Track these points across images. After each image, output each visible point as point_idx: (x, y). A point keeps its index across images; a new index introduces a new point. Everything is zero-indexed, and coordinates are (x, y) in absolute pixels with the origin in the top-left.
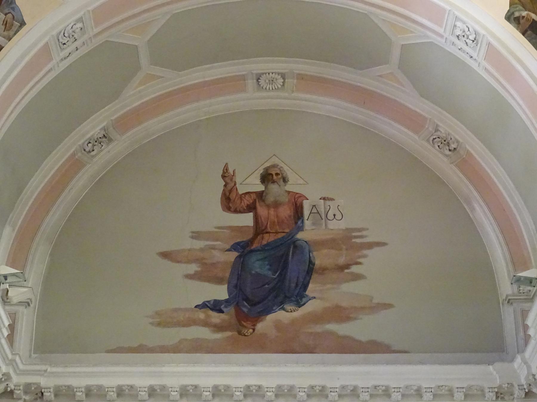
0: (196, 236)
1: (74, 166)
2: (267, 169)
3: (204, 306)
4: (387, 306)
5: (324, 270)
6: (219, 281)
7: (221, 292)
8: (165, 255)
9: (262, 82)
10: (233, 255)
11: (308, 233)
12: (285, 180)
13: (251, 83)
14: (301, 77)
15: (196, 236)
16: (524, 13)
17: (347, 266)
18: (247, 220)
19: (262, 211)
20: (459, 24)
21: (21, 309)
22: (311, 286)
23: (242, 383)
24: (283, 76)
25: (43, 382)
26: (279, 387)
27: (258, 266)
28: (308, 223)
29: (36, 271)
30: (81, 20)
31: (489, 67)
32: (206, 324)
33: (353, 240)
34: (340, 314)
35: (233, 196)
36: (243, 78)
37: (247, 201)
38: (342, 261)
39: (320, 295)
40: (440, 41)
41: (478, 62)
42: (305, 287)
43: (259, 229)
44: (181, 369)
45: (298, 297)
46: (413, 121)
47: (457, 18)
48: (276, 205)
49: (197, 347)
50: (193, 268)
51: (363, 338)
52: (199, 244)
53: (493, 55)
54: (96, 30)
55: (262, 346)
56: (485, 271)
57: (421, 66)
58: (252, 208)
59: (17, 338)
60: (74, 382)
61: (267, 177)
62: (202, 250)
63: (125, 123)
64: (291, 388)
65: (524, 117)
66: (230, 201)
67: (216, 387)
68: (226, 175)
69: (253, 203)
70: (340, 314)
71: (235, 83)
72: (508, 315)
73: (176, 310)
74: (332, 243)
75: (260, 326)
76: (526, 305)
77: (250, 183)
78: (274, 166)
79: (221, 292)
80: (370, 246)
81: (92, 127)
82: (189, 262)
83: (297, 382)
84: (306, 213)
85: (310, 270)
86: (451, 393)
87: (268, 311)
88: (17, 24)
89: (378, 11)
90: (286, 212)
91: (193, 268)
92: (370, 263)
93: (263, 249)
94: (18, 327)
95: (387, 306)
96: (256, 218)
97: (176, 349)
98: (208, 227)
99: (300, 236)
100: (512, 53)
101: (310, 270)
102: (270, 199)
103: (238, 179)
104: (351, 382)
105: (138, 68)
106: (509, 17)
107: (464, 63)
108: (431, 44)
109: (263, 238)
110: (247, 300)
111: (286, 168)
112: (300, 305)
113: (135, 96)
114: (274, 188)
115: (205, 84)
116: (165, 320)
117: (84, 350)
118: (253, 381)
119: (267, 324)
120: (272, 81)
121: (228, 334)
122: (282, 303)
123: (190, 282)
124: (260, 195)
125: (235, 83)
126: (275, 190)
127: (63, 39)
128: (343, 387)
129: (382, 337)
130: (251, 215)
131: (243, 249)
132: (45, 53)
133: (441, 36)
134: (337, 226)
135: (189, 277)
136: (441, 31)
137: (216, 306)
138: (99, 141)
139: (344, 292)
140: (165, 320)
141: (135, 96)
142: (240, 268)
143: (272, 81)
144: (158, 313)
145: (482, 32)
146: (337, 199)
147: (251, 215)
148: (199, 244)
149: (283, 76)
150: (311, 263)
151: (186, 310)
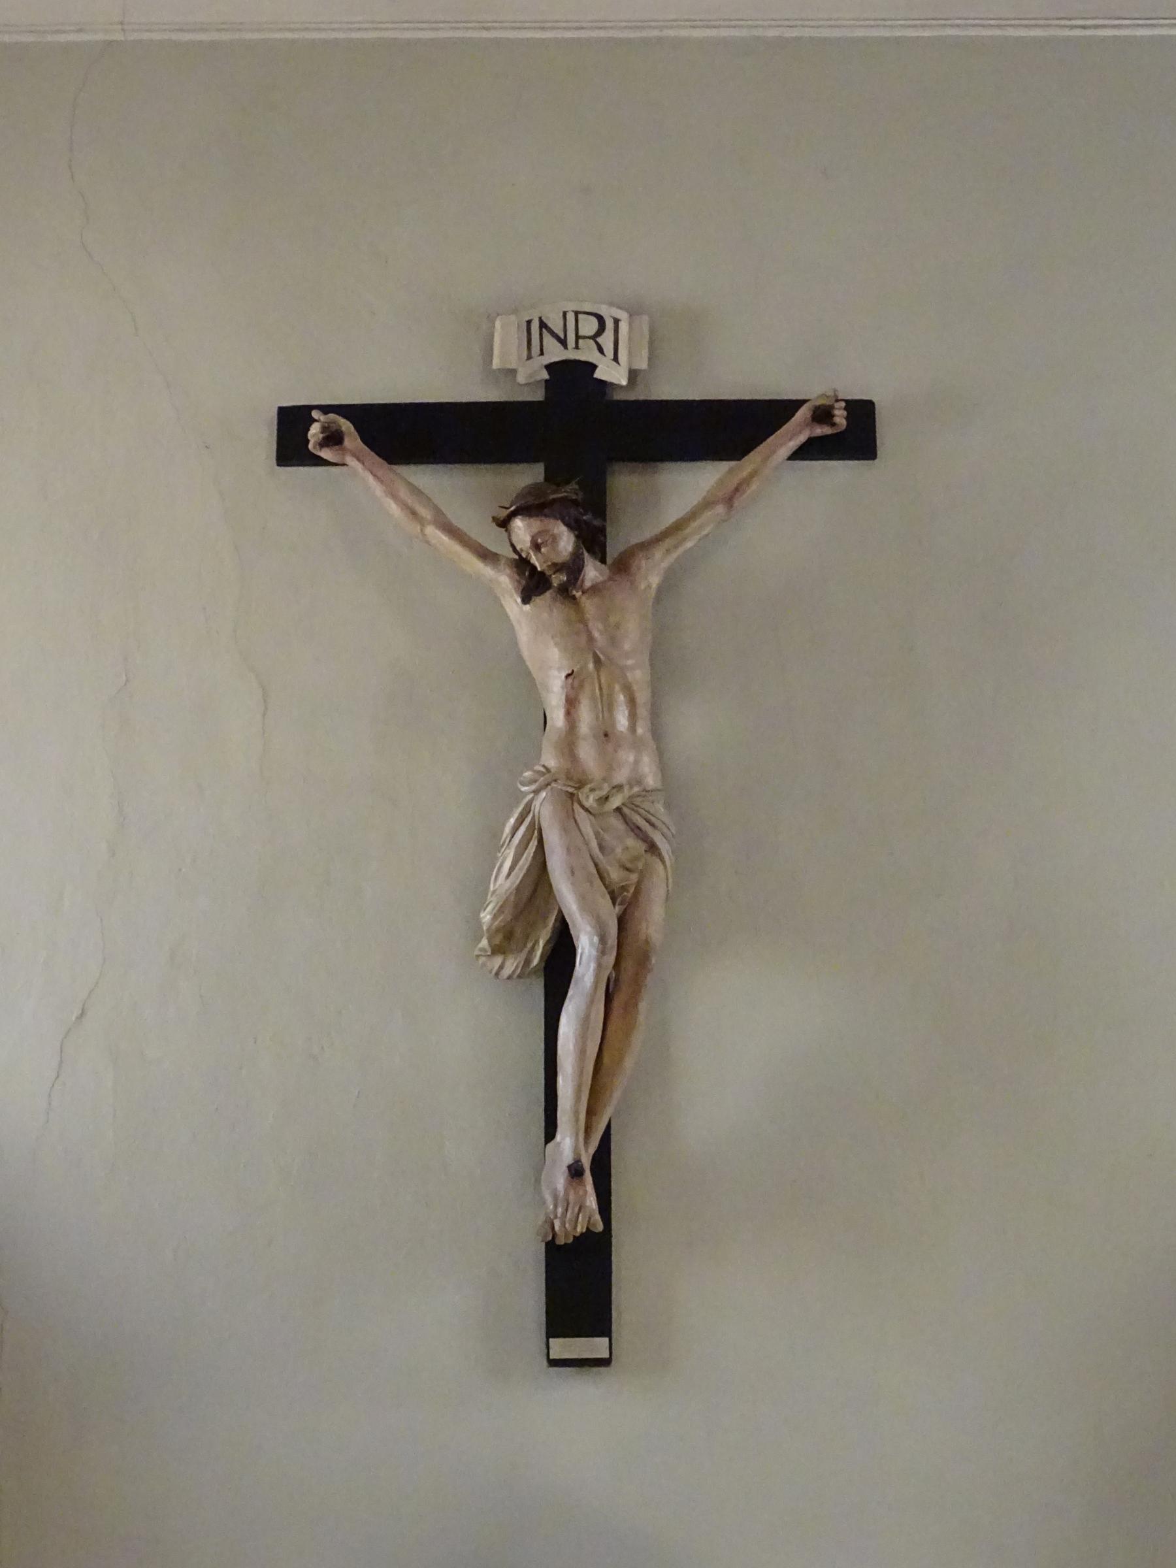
120: (333, 438)
143: (333, 438)
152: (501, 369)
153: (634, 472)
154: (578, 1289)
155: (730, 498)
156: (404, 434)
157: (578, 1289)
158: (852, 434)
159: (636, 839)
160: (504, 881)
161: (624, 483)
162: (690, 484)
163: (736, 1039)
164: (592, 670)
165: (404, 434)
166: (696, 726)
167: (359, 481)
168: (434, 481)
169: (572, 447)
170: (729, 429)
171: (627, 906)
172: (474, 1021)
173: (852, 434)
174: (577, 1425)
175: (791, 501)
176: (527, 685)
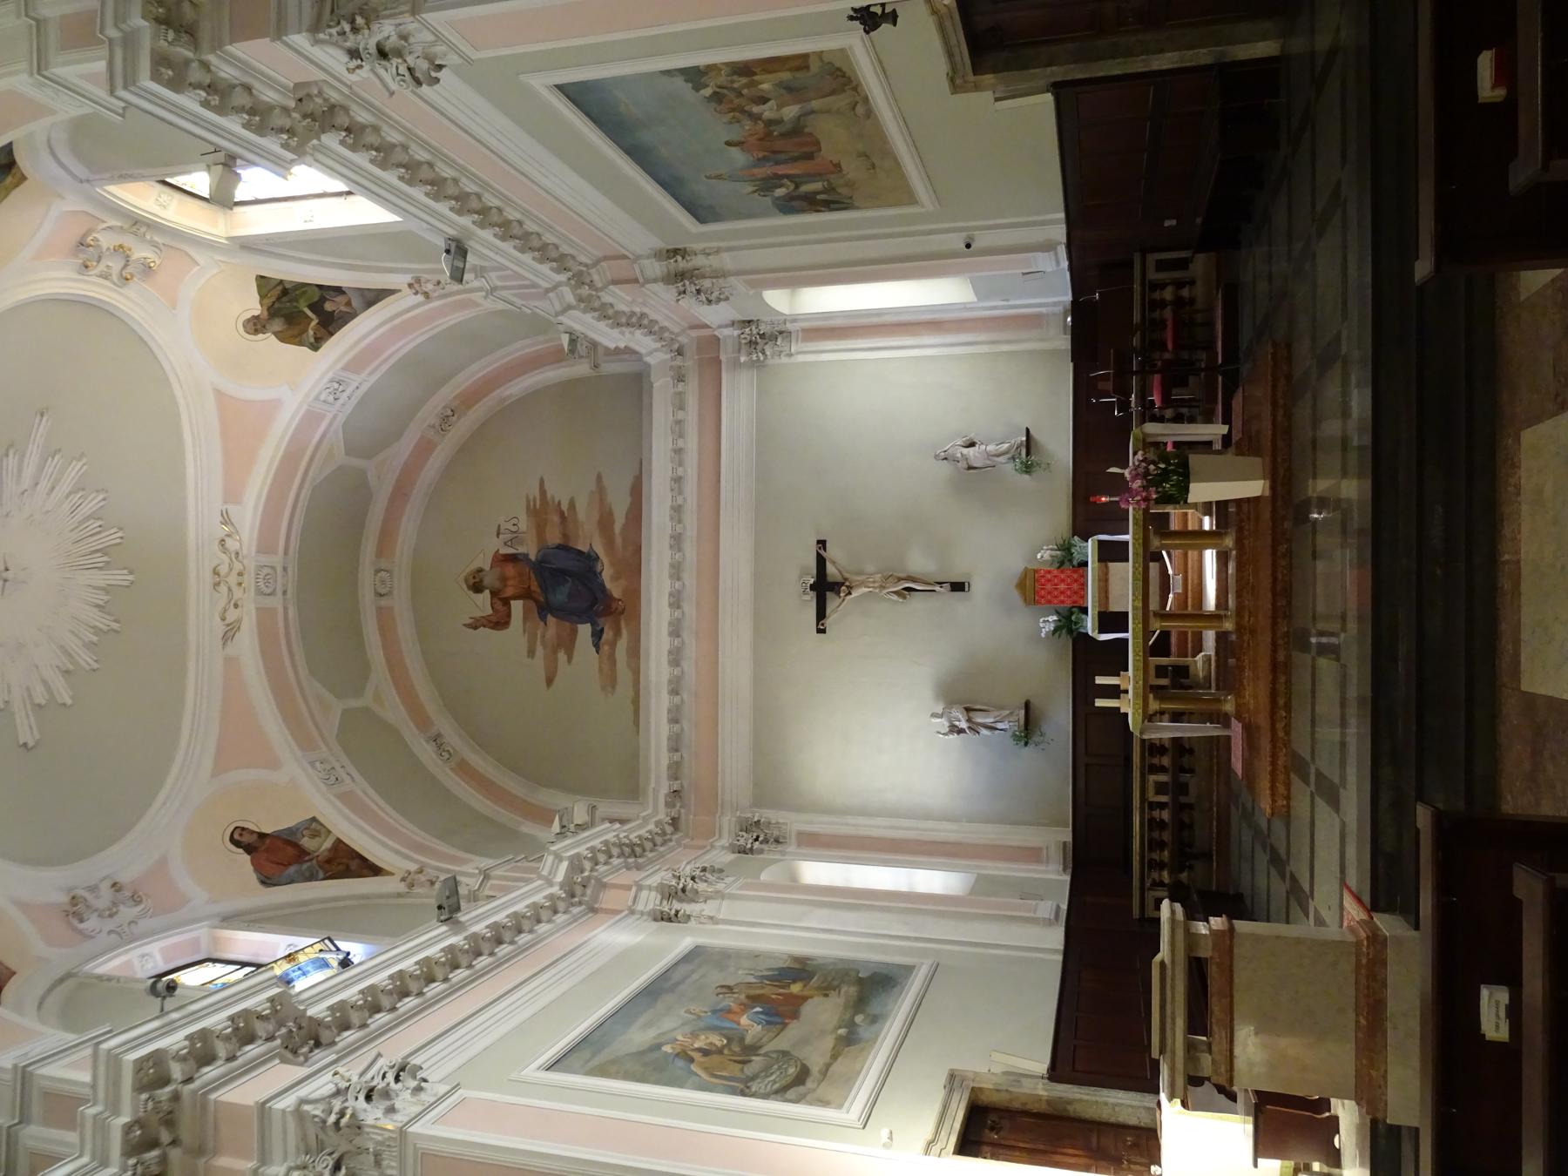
0: (531, 653)
1: (464, 769)
2: (469, 588)
3: (597, 646)
4: (599, 478)
5: (565, 536)
6: (574, 632)
7: (585, 630)
8: (550, 681)
9: (383, 591)
10: (550, 619)
11: (530, 549)
12: (480, 570)
13: (384, 602)
14: (380, 553)
15: (531, 653)
16: (311, 332)
17: (562, 514)
18: (517, 607)
19: (509, 592)
20: (323, 397)
21: (598, 814)
22: (580, 548)
23: (668, 553)
24: (377, 571)
25: (664, 790)
26: (671, 577)
27: (560, 596)
28: (522, 550)
29: (558, 800)
30: (312, 764)
31: (369, 369)
32: (613, 645)
33: (1099, 703)
34: (606, 522)
35: (494, 619)
36: (380, 610)
37: (499, 606)
38: (556, 519)
39: (588, 539)
40: (341, 418)
41: (364, 381)
42: (580, 552)
43: (526, 595)
44: (653, 665)
45: (590, 559)
46: (424, 449)
47: (317, 398)
48: (504, 579)
49: (635, 652)
50: (562, 656)
51: (629, 500)
52: (540, 651)
53: (356, 364)
54: (324, 748)
55: (634, 593)
56: (568, 388)
57: (369, 435)
58: (506, 602)
59: (624, 816)
60: (665, 762)
61: (477, 588)
62: (545, 647)
63: (422, 721)
64: (672, 566)
65: (420, 340)
66: (499, 621)
67: (670, 634)
68: (474, 626)
69: (501, 601)
70: (606, 522)
71: (385, 618)
72: (610, 368)
73: (601, 670)
74: (540, 528)
75: (616, 593)
76: (600, 351)
77: (482, 604)
78: (466, 581)
79: (585, 630)
80: (543, 492)
81: (425, 752)
82: (556, 660)
83: (667, 589)
84: (511, 551)
85: (564, 548)
86: (679, 422)
87: (602, 585)
88: (314, 825)
89: (309, 479)
90: (510, 570)
91: (562, 656)
92: (559, 492)
93: (545, 590)
94: (616, 816)
95: (599, 478)
96: (516, 598)
97: (636, 672)
98: (523, 642)
99: (533, 557)
100: (352, 348)
101: (564, 548)
102: (497, 584)
103: (478, 614)
104: (667, 512)
105: (367, 710)
106: (315, 347)
107: (366, 394)
108: (345, 426)
109: (1359, 900)
110: (593, 605)
111: (468, 570)
112: (597, 558)
113: (394, 712)
114: (487, 581)
115: (385, 647)
116: (610, 681)
117: (636, 756)
118: (665, 601)
119: (614, 588)
120: (383, 582)
121: (623, 624)
122: (595, 573)
123: (575, 660)
124: (494, 594)
125: (385, 618)
126: (490, 580)
127: (331, 779)
128: (672, 518)
129: (627, 482)
130: (513, 603)
131: (544, 609)
132: (347, 798)
133: (335, 417)
134: (524, 523)
135: (570, 659)
136: (330, 416)
137: (597, 635)
138: (439, 746)
139: (586, 516)
140: (610, 681)
141: (394, 712)
142: (563, 613)
143: (383, 582)
144: (603, 688)
145: (330, 375)
146: (498, 522)
147: (513, 603)
148: (540, 651)
149: (377, 571)
150: (559, 547)
151: (600, 662)
152: (811, 598)
153: (1048, 1102)
154: (958, 587)
155: (834, 563)
156: (821, 614)
157: (958, 587)
158: (822, 543)
159: (889, 578)
160: (895, 597)
161: (830, 579)
162: (830, 569)
163: (919, 562)
164: (863, 584)
165: (821, 614)
166: (870, 568)
167: (828, 622)
168: (828, 611)
169: (824, 587)
170: (821, 562)
171: (900, 579)
172: (917, 603)
173: (822, 543)
174: (978, 587)
175: (832, 553)
176: (863, 595)
